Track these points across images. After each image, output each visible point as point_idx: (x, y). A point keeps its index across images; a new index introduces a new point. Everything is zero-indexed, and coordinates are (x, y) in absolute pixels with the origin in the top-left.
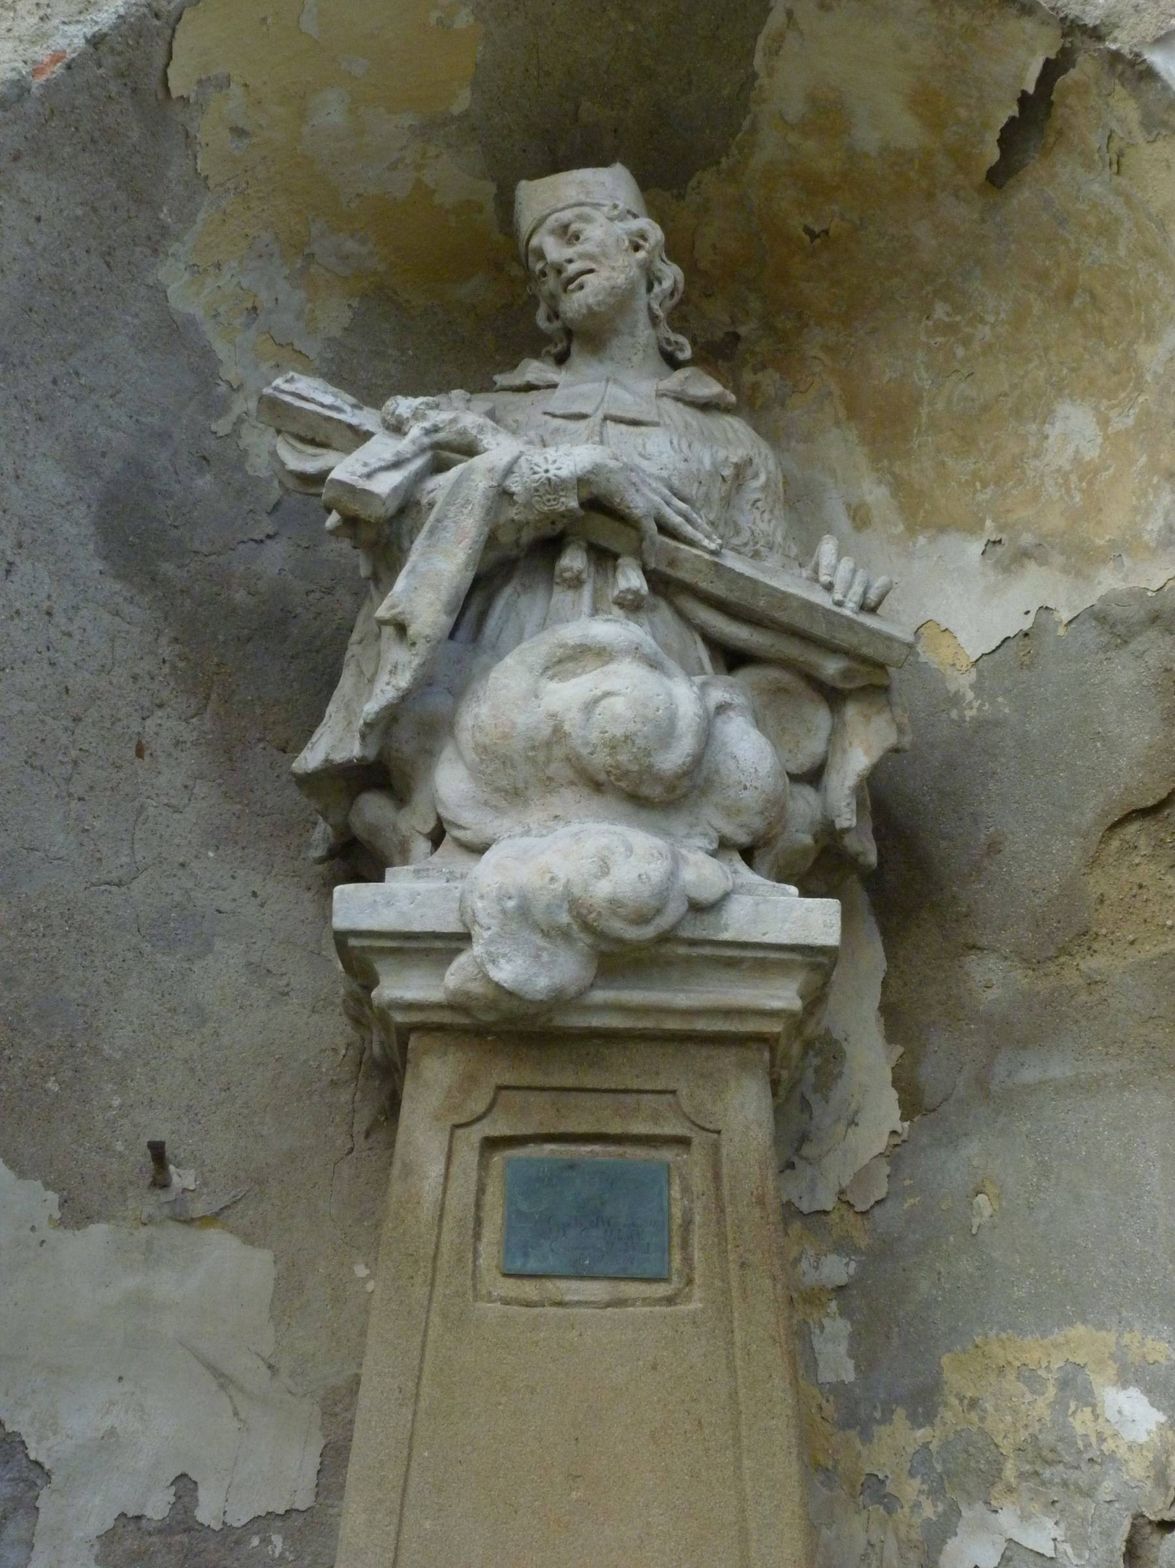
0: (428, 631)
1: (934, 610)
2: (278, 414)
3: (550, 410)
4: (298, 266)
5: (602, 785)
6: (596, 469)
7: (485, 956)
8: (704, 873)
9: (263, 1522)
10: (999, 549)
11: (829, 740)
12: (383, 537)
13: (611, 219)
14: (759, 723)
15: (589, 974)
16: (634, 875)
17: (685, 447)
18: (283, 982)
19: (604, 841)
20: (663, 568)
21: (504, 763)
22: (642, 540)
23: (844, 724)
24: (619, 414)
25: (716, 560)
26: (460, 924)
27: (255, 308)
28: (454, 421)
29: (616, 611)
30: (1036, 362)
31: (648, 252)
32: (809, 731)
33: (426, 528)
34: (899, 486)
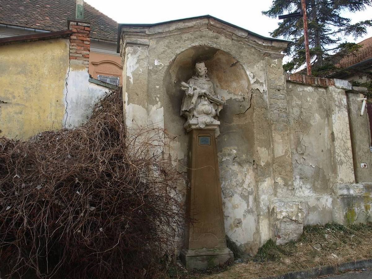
9: (181, 159)
34: (220, 85)
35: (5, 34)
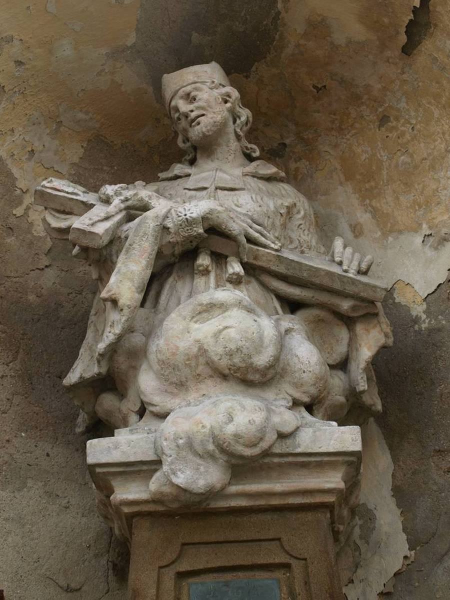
0: (128, 303)
1: (401, 274)
2: (43, 197)
3: (188, 187)
4: (54, 128)
5: (227, 376)
6: (211, 212)
7: (169, 471)
8: (287, 419)
10: (431, 239)
11: (349, 345)
12: (102, 256)
13: (211, 89)
14: (310, 338)
15: (226, 478)
16: (246, 421)
17: (259, 200)
18: (66, 501)
19: (229, 404)
20: (252, 261)
21: (174, 369)
22: (239, 246)
23: (356, 335)
24: (223, 185)
25: (279, 254)
26: (155, 456)
27: (33, 150)
28: (136, 195)
29: (228, 285)
30: (439, 140)
31: (232, 103)
32: (338, 341)
33: (124, 249)
34: (375, 213)
35: (263, 507)
